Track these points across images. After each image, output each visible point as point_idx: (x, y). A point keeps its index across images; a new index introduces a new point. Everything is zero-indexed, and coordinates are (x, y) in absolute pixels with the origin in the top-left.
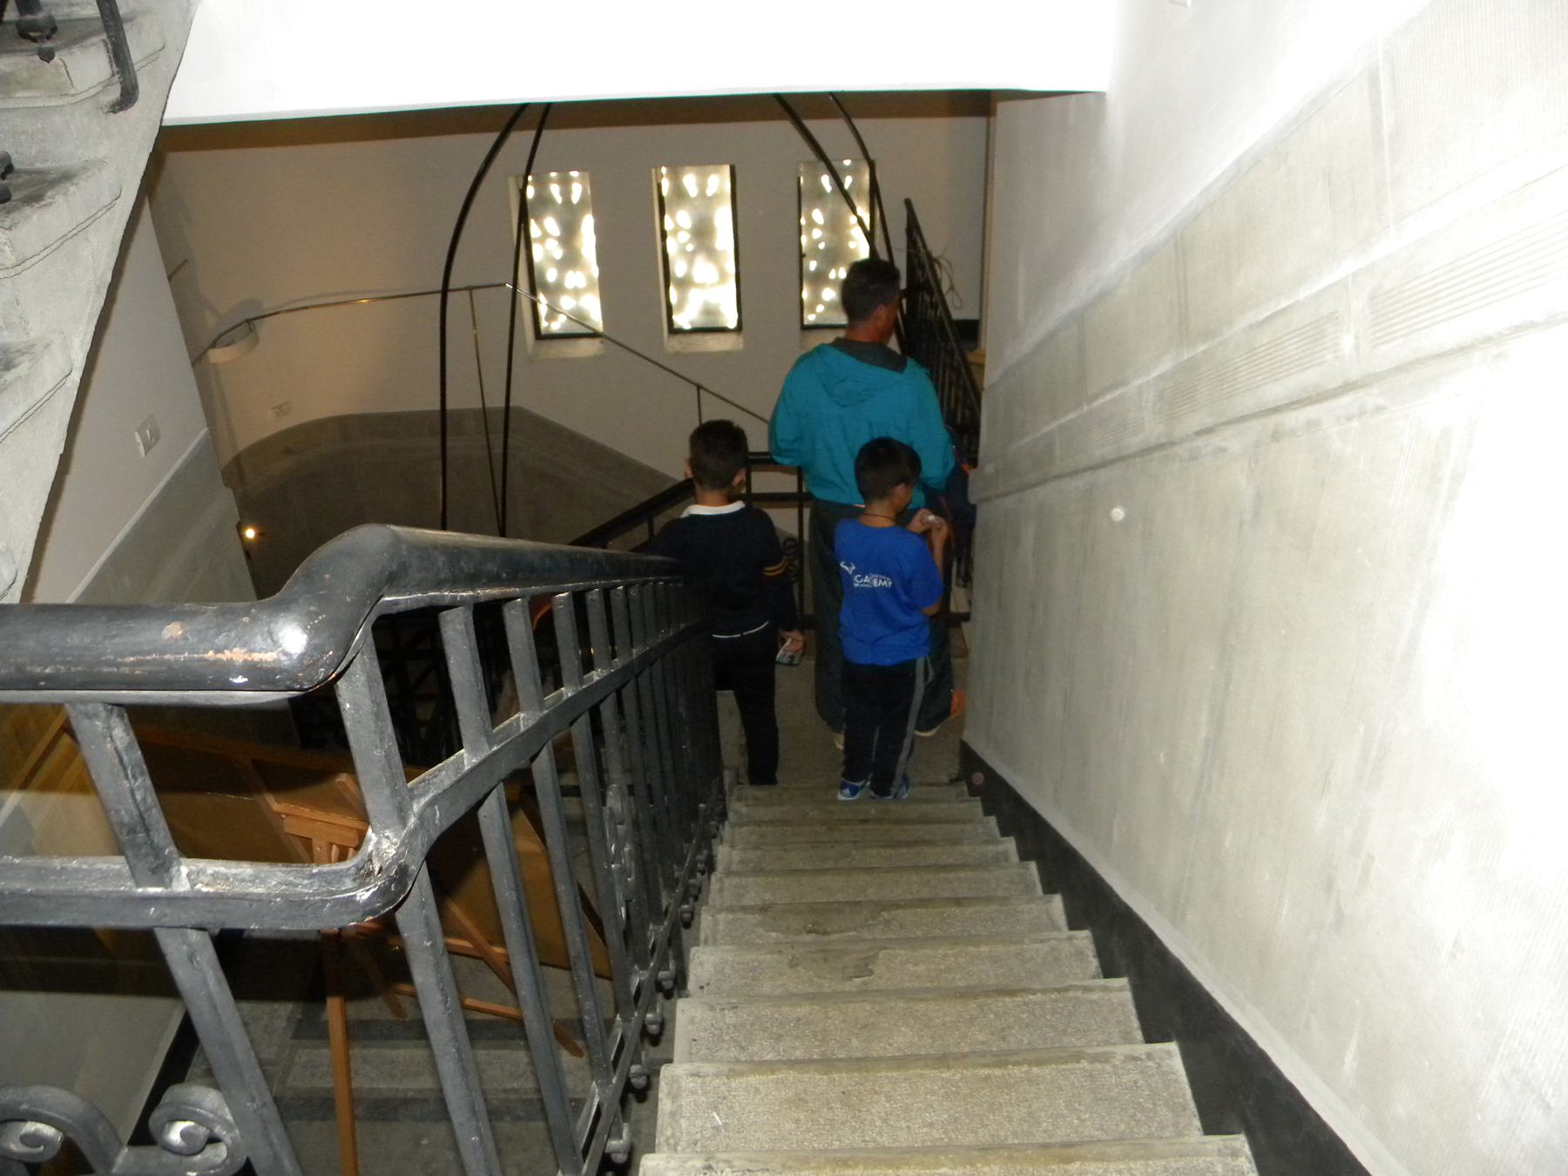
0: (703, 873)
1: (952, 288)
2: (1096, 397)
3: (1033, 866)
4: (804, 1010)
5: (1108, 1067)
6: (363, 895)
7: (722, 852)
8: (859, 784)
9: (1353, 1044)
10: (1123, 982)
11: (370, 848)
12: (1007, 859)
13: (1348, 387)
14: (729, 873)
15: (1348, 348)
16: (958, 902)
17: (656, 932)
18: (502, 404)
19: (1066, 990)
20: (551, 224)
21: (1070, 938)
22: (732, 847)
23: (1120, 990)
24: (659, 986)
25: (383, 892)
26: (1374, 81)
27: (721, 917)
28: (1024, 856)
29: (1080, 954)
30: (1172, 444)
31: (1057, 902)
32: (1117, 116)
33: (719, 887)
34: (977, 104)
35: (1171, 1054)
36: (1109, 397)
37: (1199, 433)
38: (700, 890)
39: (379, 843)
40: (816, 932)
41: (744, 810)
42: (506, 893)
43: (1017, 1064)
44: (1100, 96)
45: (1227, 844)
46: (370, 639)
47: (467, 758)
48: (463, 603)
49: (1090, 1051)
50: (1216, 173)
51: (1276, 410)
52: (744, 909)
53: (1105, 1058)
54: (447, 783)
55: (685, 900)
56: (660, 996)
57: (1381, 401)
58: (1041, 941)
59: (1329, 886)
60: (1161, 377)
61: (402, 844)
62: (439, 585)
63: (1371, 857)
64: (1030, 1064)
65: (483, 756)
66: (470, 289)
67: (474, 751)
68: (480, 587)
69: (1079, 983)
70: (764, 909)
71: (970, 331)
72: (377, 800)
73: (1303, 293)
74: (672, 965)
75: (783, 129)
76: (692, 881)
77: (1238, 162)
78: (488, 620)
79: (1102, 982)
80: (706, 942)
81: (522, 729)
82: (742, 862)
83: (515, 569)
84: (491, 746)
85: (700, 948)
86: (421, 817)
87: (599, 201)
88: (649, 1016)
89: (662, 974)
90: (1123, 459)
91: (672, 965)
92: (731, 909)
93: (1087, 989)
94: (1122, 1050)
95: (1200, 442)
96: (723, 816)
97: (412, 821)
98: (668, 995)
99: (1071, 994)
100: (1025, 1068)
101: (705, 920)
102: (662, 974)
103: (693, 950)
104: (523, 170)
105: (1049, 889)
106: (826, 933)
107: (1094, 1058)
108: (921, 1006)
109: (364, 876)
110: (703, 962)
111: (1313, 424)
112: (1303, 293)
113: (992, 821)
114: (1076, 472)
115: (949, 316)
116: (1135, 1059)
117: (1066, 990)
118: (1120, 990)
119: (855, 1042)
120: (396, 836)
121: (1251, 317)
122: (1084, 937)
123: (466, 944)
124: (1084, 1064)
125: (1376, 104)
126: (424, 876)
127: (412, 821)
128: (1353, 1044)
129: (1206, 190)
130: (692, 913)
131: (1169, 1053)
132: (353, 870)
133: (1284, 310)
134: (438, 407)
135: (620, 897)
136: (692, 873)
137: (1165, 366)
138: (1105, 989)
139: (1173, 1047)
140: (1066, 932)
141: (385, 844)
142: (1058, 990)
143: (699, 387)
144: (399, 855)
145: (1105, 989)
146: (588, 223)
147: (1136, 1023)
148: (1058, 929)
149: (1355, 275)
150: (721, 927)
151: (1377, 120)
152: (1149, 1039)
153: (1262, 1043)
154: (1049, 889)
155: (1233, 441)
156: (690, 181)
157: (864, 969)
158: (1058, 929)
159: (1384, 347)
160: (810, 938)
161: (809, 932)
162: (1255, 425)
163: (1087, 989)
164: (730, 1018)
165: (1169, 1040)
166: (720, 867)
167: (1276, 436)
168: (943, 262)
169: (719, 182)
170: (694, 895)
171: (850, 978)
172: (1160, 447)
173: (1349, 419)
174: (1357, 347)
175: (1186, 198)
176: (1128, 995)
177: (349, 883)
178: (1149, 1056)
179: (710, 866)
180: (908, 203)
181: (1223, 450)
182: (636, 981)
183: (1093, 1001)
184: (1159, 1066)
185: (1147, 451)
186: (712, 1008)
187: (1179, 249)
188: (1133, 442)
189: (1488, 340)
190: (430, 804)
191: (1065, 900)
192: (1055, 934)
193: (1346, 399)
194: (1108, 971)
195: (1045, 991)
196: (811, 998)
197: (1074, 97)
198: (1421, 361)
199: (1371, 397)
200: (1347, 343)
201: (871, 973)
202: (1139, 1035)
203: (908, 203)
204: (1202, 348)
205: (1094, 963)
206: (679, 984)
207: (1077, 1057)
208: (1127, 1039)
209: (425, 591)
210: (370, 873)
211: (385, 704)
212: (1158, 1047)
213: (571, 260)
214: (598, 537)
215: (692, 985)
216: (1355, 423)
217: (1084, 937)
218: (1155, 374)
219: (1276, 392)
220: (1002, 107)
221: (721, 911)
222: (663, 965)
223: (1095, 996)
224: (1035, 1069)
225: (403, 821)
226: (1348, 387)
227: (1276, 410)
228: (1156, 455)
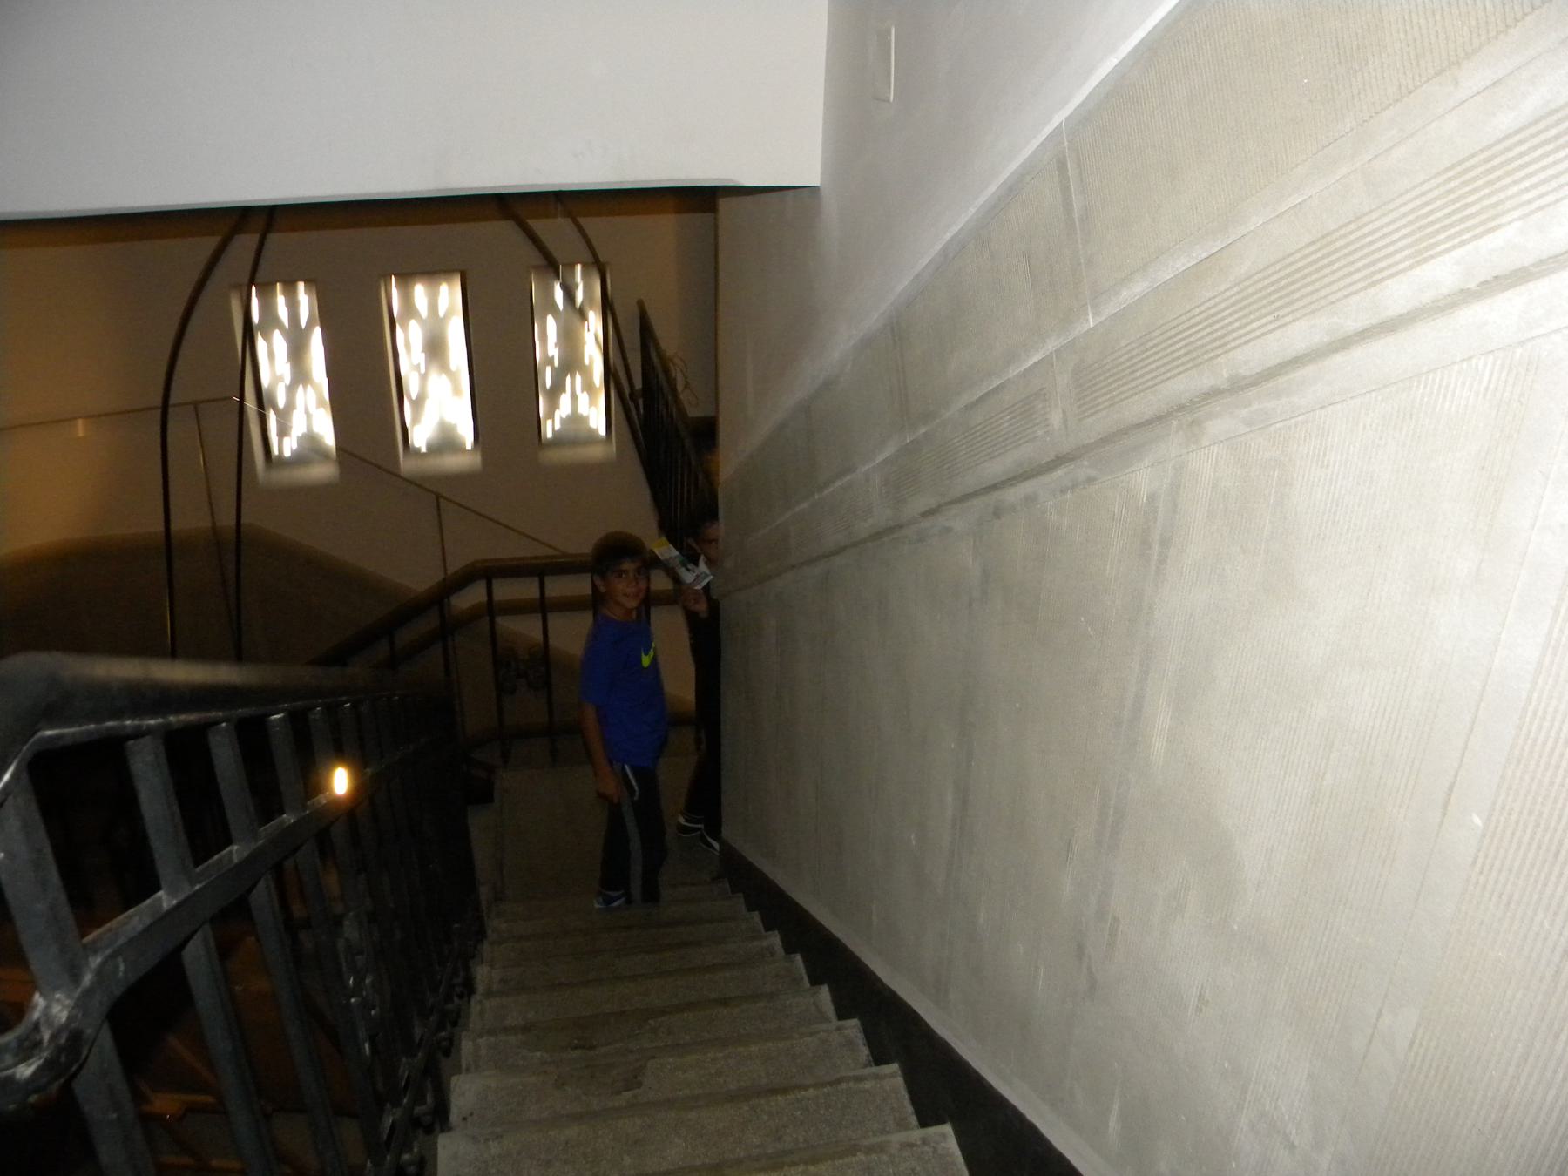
0: (461, 996)
1: (687, 386)
2: (826, 484)
3: (798, 958)
4: (571, 1132)
5: (885, 1158)
6: (25, 1071)
7: (482, 973)
8: (614, 894)
9: (1116, 1107)
10: (894, 1067)
11: (36, 1015)
12: (772, 954)
13: (1060, 460)
14: (489, 994)
15: (1058, 423)
16: (724, 1002)
17: (406, 1068)
18: (233, 522)
19: (839, 1081)
20: (279, 342)
21: (839, 1029)
22: (492, 966)
23: (893, 1075)
24: (416, 1123)
25: (48, 1065)
26: (1062, 166)
27: (482, 1041)
28: (789, 949)
29: (850, 1044)
30: (901, 527)
31: (824, 993)
32: (831, 207)
33: (479, 1010)
34: (700, 200)
35: (945, 1137)
36: (838, 483)
37: (925, 515)
38: (459, 1016)
39: (48, 1007)
40: (583, 1047)
41: (504, 926)
42: (220, 1041)
43: (794, 1164)
44: (813, 190)
45: (981, 920)
46: (25, 776)
47: (165, 899)
48: (150, 731)
49: (866, 1142)
50: (926, 261)
51: (995, 487)
52: (507, 1030)
53: (881, 1148)
54: (140, 928)
55: (441, 1026)
56: (420, 1131)
57: (1092, 473)
58: (811, 1034)
59: (1080, 949)
60: (885, 462)
61: (76, 1006)
62: (118, 714)
63: (1116, 919)
64: (806, 1163)
65: (182, 897)
66: (196, 405)
67: (172, 894)
68: (172, 713)
69: (851, 1074)
70: (526, 1029)
71: (707, 432)
72: (42, 959)
73: (1013, 372)
74: (429, 1099)
75: (504, 230)
76: (450, 1006)
77: (945, 249)
78: (186, 751)
79: (874, 1069)
80: (468, 1070)
81: (236, 860)
82: (503, 981)
83: (269, 696)
84: (192, 884)
85: (462, 1077)
86: (99, 972)
87: (327, 315)
88: (406, 1157)
89: (418, 1110)
90: (855, 545)
91: (429, 1099)
92: (491, 1032)
93: (859, 1079)
94: (897, 1138)
95: (925, 524)
96: (481, 934)
97: (88, 979)
98: (429, 1130)
99: (844, 1086)
100: (801, 1168)
101: (466, 1046)
102: (418, 1110)
103: (454, 1079)
104: (246, 281)
105: (816, 981)
106: (592, 1048)
107: (870, 1150)
108: (692, 1115)
109: (27, 1049)
110: (465, 1092)
111: (1030, 499)
112: (1013, 372)
113: (756, 917)
114: (811, 561)
115: (682, 411)
116: (911, 1145)
117: (839, 1081)
118: (893, 1075)
119: (627, 1160)
120: (68, 997)
121: (967, 398)
122: (853, 1026)
123: (210, 1099)
124: (861, 1156)
125: (1066, 189)
126: (106, 1040)
127: (88, 979)
128: (1116, 1107)
129: (917, 276)
130: (451, 1040)
131: (944, 1136)
132: (14, 1045)
133: (997, 390)
134: (160, 528)
135: (362, 1034)
136: (448, 999)
137: (889, 450)
138: (877, 1077)
139: (947, 1129)
140: (835, 1023)
141: (56, 1009)
142: (831, 1084)
143: (438, 496)
144: (70, 1018)
145: (877, 1077)
146: (316, 339)
147: (910, 1109)
148: (828, 1020)
149: (1058, 351)
150: (483, 1052)
151: (1067, 204)
152: (924, 1124)
153: (1032, 1117)
154: (816, 981)
155: (959, 521)
156: (420, 291)
157: (633, 1082)
158: (828, 1020)
159: (1090, 420)
160: (576, 1054)
161: (576, 1048)
162: (976, 502)
163: (859, 1079)
164: (495, 1148)
165: (944, 1122)
166: (480, 988)
167: (997, 513)
168: (677, 360)
169: (449, 295)
170: (454, 1020)
171: (619, 1093)
172: (890, 530)
173: (1063, 491)
174: (1065, 421)
175: (902, 284)
176: (900, 1081)
177: (9, 1059)
178: (925, 1141)
179: (469, 988)
180: (641, 304)
181: (949, 530)
182: (388, 1121)
183: (867, 1091)
184: (935, 1150)
185: (877, 536)
186: (475, 1139)
187: (897, 331)
188: (863, 527)
189: (1181, 408)
190: (113, 956)
191: (831, 991)
192: (824, 1026)
193: (1060, 472)
194: (879, 1059)
195: (815, 1086)
196: (577, 1118)
197: (791, 192)
198: (1125, 431)
199: (1083, 469)
200: (1056, 418)
201: (640, 1085)
202: (913, 1120)
203: (641, 304)
204: (923, 430)
205: (865, 1051)
206: (440, 1118)
207: (853, 1150)
208: (902, 1125)
209: (99, 721)
210: (37, 1044)
211: (48, 850)
212: (932, 1131)
213: (300, 375)
214: (338, 657)
215: (454, 1117)
216: (1069, 495)
217: (853, 1026)
218: (880, 458)
219: (994, 469)
220: (724, 204)
221: (481, 1036)
222: (419, 1099)
223: (868, 1085)
224: (812, 1168)
225: (76, 978)
226: (1060, 460)
227: (995, 487)
228: (886, 539)
